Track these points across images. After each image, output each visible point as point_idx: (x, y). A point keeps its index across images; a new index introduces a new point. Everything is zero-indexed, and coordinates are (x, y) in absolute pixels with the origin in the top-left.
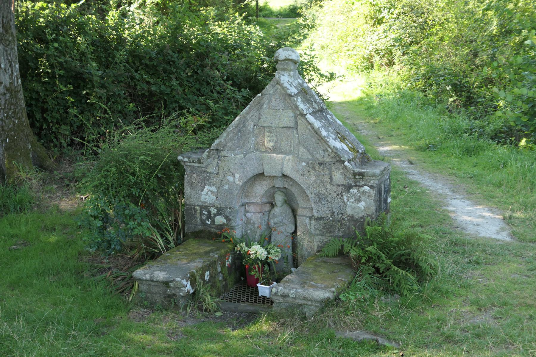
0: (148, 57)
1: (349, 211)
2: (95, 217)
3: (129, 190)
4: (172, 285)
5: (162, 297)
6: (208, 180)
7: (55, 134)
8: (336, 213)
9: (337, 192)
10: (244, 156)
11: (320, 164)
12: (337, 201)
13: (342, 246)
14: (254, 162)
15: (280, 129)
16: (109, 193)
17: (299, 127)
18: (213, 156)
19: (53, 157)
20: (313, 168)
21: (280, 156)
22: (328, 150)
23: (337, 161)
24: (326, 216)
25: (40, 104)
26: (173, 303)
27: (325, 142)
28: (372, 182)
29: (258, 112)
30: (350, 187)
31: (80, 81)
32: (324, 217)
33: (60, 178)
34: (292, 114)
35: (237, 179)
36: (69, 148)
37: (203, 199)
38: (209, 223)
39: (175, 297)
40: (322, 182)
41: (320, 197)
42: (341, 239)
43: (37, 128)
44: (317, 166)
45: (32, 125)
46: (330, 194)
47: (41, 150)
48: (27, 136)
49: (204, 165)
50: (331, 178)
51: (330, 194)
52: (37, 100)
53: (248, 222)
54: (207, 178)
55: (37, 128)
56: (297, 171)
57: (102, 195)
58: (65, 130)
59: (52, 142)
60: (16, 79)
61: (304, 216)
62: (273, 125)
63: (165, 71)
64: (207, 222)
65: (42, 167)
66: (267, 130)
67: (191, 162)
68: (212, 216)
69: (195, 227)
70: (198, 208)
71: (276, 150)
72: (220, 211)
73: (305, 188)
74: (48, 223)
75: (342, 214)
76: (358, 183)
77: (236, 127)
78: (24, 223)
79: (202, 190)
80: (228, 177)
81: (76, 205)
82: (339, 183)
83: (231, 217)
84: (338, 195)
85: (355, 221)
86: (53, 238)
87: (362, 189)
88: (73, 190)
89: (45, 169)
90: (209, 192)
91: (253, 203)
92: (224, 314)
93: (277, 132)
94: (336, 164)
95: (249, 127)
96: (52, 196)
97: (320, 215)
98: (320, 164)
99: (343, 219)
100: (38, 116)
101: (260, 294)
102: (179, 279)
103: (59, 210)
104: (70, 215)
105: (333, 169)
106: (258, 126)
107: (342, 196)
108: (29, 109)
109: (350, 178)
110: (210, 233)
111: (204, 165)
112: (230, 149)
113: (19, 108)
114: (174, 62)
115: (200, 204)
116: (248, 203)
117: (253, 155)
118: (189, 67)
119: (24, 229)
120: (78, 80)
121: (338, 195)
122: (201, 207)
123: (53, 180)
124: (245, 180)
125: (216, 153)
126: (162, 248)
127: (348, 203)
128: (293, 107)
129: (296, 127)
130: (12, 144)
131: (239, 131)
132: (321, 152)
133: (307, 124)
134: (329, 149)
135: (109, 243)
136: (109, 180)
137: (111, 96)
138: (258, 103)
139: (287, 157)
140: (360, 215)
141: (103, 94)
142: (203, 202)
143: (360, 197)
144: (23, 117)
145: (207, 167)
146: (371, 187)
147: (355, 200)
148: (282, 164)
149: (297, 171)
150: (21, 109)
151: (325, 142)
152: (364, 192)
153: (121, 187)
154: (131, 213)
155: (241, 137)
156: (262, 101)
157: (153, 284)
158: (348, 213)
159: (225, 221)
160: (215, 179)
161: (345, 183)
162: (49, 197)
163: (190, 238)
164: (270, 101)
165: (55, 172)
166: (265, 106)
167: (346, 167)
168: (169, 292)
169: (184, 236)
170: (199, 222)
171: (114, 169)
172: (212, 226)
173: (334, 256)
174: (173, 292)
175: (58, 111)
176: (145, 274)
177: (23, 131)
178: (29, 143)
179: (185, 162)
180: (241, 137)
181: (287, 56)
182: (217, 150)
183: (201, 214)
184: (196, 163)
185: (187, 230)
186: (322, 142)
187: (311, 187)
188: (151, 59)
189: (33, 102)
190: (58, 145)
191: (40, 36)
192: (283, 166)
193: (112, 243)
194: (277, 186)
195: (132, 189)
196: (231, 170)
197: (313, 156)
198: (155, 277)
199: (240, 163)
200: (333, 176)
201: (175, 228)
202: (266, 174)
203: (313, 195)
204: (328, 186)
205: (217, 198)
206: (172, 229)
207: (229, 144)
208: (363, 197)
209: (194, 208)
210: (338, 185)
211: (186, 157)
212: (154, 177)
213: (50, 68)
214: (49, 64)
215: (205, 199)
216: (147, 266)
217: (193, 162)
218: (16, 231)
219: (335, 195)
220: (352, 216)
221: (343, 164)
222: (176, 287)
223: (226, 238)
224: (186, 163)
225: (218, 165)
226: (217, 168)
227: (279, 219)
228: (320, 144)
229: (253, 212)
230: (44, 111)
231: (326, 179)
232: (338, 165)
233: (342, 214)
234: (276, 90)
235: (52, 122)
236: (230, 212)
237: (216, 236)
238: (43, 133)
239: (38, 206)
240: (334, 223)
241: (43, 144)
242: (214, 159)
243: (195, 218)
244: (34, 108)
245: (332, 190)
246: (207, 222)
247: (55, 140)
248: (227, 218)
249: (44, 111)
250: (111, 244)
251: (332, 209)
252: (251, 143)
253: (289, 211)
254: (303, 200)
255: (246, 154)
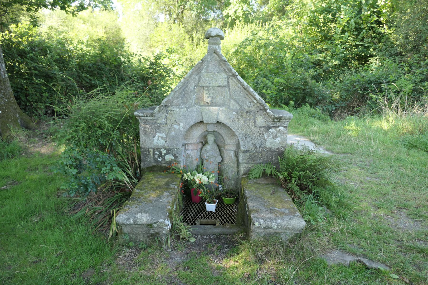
0: (88, 66)
1: (268, 145)
2: (71, 166)
3: (97, 140)
4: (155, 225)
5: (145, 236)
6: (159, 129)
7: (35, 108)
8: (258, 147)
9: (259, 132)
10: (187, 110)
11: (247, 112)
12: (259, 138)
13: (264, 170)
14: (194, 114)
15: (216, 88)
16: (81, 144)
17: (231, 86)
18: (163, 111)
19: (35, 121)
20: (242, 116)
21: (216, 108)
22: (253, 102)
23: (260, 109)
24: (250, 150)
25: (24, 91)
26: (157, 241)
27: (252, 95)
28: (286, 123)
29: (198, 76)
30: (269, 128)
31: (48, 79)
32: (249, 151)
33: (40, 134)
34: (226, 76)
35: (182, 126)
36: (45, 116)
37: (155, 143)
38: (161, 160)
39: (158, 236)
40: (248, 125)
41: (246, 136)
42: (262, 165)
43: (23, 105)
44: (244, 114)
45: (19, 104)
46: (254, 134)
47: (25, 116)
48: (15, 109)
49: (155, 118)
50: (255, 122)
51: (254, 134)
52: (22, 89)
53: (188, 157)
54: (157, 128)
55: (23, 105)
56: (229, 119)
57: (75, 146)
58: (41, 106)
59: (34, 113)
60: (3, 73)
61: (229, 150)
62: (211, 85)
63: (98, 73)
64: (159, 159)
65: (27, 128)
66: (206, 89)
67: (145, 116)
68: (163, 155)
69: (149, 164)
70: (151, 150)
71: (212, 104)
72: (169, 152)
73: (234, 131)
74: (32, 164)
75: (263, 148)
76: (275, 125)
77: (181, 88)
78: (13, 167)
79: (154, 137)
80: (175, 126)
81: (52, 150)
82: (261, 126)
83: (177, 155)
84: (260, 134)
85: (272, 151)
86: (36, 176)
87: (278, 129)
88: (49, 141)
89: (30, 129)
90: (160, 138)
91: (191, 143)
92: (196, 238)
93: (214, 90)
94: (259, 112)
95: (191, 88)
96: (35, 145)
97: (246, 149)
98: (247, 112)
99: (264, 151)
100: (23, 98)
101: (207, 210)
102: (162, 220)
103: (41, 155)
104: (49, 157)
105: (257, 115)
106: (198, 86)
107: (263, 135)
108: (17, 94)
109: (270, 122)
110: (161, 167)
111: (155, 118)
112: (176, 105)
113: (8, 92)
114: (103, 69)
115: (153, 147)
116: (186, 144)
117: (194, 108)
118: (112, 71)
119: (14, 170)
120: (49, 77)
121: (260, 134)
122: (153, 149)
123: (35, 135)
124: (188, 127)
125: (165, 109)
126: (128, 183)
127: (268, 139)
128: (227, 70)
129: (228, 86)
130: (5, 114)
131: (183, 91)
132: (248, 104)
133: (237, 83)
134: (255, 101)
135: (86, 187)
136: (80, 134)
137: (68, 86)
138: (199, 68)
139: (221, 109)
140: (276, 147)
141: (63, 85)
142: (155, 145)
143: (277, 134)
144: (11, 97)
145: (157, 119)
146: (285, 127)
147: (273, 137)
148: (218, 114)
149: (229, 119)
150: (9, 93)
151: (252, 95)
152: (280, 131)
153: (90, 138)
154: (101, 160)
155: (184, 95)
156: (202, 67)
157: (137, 226)
158: (267, 147)
159: (173, 158)
160: (165, 128)
161: (265, 125)
162: (33, 146)
163: (146, 172)
164: (208, 66)
165: (36, 130)
166: (204, 70)
167: (268, 114)
168: (152, 232)
169: (140, 171)
170: (152, 160)
171: (83, 125)
172: (163, 162)
173: (259, 178)
174: (156, 231)
175: (36, 95)
176: (128, 219)
177: (11, 106)
178: (17, 113)
179: (140, 116)
180: (184, 95)
181: (218, 33)
182: (166, 106)
183: (154, 154)
184: (149, 116)
185: (141, 167)
186: (250, 96)
187: (240, 129)
188: (90, 67)
189: (19, 90)
190: (38, 115)
191: (22, 54)
192: (218, 116)
193: (88, 187)
194: (209, 130)
195: (100, 140)
196: (177, 120)
197: (241, 106)
198: (139, 220)
199: (184, 115)
200: (257, 121)
201: (132, 165)
202: (205, 122)
203: (241, 135)
204: (253, 128)
205: (166, 142)
206: (130, 165)
207: (175, 101)
208: (279, 135)
209: (148, 150)
210: (260, 127)
211: (141, 113)
212: (117, 130)
213: (29, 70)
214: (28, 68)
215: (157, 143)
216: (126, 208)
217: (147, 116)
218: (8, 173)
219: (258, 134)
220: (271, 149)
221: (266, 111)
222: (158, 227)
223: (174, 169)
224: (141, 117)
225: (166, 118)
226: (166, 120)
227: (211, 153)
228: (247, 98)
229: (191, 150)
230: (27, 95)
231: (252, 123)
232: (261, 112)
233: (263, 148)
234: (213, 57)
235: (32, 101)
236: (177, 151)
237: (167, 169)
238: (27, 108)
239: (26, 153)
240: (257, 154)
241: (28, 115)
242: (163, 113)
243: (149, 158)
244: (20, 94)
245: (256, 131)
246: (159, 159)
247: (35, 112)
248: (175, 156)
249: (27, 95)
250: (87, 189)
251: (255, 144)
252: (193, 98)
253: (216, 147)
254: (229, 139)
255: (189, 108)
